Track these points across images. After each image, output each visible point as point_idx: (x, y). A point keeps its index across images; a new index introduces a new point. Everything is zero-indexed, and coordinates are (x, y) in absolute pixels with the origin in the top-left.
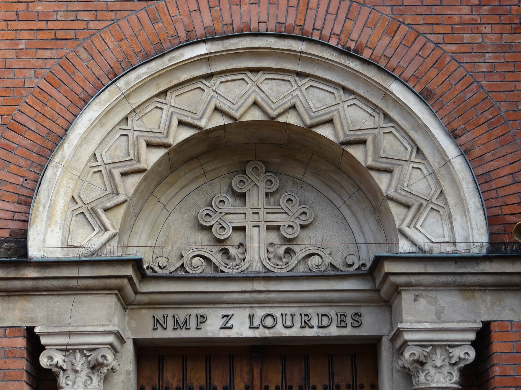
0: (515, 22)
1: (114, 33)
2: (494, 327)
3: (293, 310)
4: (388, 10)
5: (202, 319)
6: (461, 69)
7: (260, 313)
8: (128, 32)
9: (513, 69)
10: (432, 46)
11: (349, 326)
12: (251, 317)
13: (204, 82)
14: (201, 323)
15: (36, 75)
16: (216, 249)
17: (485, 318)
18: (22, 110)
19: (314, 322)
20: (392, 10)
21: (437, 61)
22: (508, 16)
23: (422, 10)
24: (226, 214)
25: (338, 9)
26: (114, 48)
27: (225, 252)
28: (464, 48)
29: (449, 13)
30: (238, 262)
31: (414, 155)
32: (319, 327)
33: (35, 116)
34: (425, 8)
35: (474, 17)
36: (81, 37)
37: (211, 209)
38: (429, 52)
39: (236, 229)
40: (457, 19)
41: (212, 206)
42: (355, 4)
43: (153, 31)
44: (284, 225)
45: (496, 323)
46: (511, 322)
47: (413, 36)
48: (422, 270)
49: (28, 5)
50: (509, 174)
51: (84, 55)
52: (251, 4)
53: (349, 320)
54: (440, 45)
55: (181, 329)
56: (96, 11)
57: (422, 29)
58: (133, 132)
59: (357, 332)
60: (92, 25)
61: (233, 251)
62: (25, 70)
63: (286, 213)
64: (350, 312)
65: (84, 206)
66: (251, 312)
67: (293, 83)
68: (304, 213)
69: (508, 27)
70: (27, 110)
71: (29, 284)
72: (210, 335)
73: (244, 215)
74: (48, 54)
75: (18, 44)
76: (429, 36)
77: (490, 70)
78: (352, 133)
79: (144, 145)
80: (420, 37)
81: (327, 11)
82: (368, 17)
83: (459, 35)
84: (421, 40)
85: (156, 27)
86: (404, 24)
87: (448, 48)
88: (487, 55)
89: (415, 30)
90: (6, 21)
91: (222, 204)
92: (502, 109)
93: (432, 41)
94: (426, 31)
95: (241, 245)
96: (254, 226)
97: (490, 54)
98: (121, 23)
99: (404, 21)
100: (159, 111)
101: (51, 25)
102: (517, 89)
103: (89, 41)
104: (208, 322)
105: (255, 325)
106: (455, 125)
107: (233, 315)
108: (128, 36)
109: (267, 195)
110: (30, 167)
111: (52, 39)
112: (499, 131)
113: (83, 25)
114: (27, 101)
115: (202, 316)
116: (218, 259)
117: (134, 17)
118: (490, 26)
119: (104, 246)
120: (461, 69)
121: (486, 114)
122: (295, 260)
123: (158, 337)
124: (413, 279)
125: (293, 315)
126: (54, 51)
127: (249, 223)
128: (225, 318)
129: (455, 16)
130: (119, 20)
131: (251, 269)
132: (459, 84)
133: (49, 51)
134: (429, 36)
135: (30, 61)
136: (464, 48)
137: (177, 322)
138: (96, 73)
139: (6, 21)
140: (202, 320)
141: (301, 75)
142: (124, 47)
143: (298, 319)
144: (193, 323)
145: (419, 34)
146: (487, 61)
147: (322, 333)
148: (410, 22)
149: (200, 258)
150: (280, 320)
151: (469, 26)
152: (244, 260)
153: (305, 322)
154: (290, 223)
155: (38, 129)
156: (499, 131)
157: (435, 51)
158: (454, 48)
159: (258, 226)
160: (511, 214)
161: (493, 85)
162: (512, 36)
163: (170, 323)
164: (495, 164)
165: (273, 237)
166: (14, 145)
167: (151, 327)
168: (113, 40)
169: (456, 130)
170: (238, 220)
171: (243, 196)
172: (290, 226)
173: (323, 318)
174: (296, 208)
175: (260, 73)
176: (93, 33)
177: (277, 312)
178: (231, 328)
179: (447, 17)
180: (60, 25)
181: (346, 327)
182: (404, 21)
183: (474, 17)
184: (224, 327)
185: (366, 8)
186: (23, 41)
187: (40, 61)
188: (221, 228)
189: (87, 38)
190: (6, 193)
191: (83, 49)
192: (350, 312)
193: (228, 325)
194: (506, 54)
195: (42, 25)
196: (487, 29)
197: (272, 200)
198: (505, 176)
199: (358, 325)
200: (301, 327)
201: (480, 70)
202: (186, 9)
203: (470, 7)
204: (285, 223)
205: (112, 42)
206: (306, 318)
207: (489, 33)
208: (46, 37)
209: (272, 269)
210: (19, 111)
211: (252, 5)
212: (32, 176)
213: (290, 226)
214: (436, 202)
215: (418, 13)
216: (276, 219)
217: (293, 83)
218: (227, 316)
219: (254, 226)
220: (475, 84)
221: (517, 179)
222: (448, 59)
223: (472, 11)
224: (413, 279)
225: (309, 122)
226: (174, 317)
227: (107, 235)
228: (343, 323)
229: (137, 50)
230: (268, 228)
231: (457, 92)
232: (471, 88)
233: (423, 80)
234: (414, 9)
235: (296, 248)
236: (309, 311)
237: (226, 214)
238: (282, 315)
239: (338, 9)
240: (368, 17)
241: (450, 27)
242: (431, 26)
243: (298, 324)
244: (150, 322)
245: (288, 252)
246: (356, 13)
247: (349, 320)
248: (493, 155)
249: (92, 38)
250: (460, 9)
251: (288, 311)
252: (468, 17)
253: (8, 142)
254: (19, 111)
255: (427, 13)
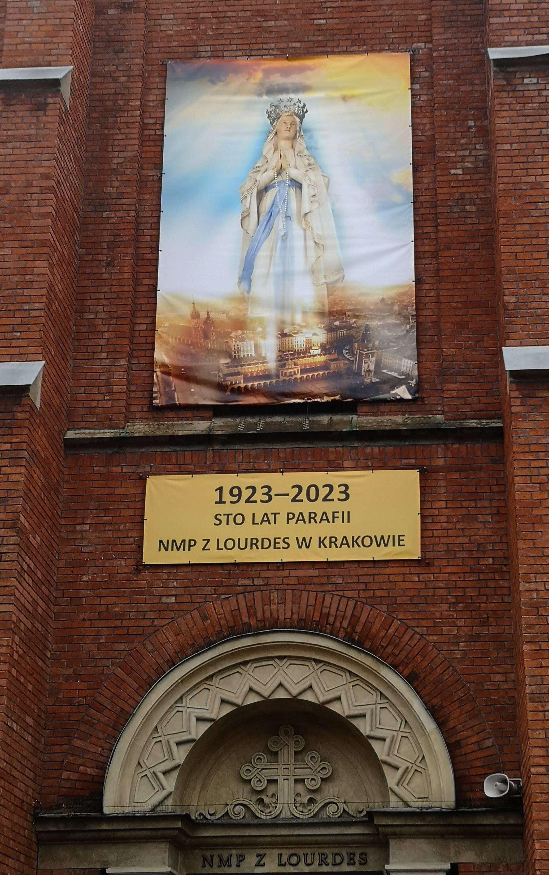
0: (484, 616)
1: (173, 629)
2: (461, 869)
3: (313, 850)
4: (384, 608)
5: (241, 859)
6: (441, 656)
7: (286, 853)
8: (184, 628)
9: (480, 656)
10: (418, 636)
11: (357, 863)
12: (280, 855)
13: (242, 667)
14: (240, 861)
15: (113, 664)
16: (254, 798)
17: (455, 861)
18: (102, 693)
19: (330, 860)
20: (388, 608)
21: (422, 649)
22: (478, 612)
23: (410, 607)
24: (263, 769)
25: (346, 607)
26: (173, 642)
27: (261, 801)
28: (442, 639)
29: (432, 610)
30: (271, 809)
31: (403, 726)
32: (333, 865)
33: (112, 697)
34: (413, 605)
35: (451, 613)
36: (148, 632)
37: (251, 765)
38: (416, 642)
39: (269, 781)
40: (438, 615)
41: (251, 763)
42: (359, 603)
43: (203, 627)
44: (308, 779)
45: (462, 865)
46: (473, 864)
47: (403, 629)
48: (403, 823)
49: (108, 607)
50: (475, 742)
51: (150, 647)
52: (280, 604)
53: (357, 858)
54: (424, 636)
55: (225, 866)
56: (160, 611)
57: (411, 623)
58: (186, 708)
59: (363, 869)
60: (156, 623)
61: (267, 800)
62: (104, 661)
63: (310, 768)
64: (358, 852)
65: (148, 770)
66: (280, 851)
67: (311, 668)
68: (324, 768)
69: (477, 621)
70: (106, 692)
71: (104, 834)
72: (247, 871)
73: (276, 770)
74: (122, 646)
75: (99, 639)
76: (416, 629)
77: (462, 656)
78: (276, 767)
79: (195, 720)
80: (409, 630)
81: (338, 609)
82: (369, 614)
83: (439, 628)
84: (410, 632)
85: (205, 624)
86: (397, 619)
87: (430, 638)
88: (461, 644)
89: (405, 624)
90: (90, 620)
91: (259, 760)
92: (471, 689)
93: (418, 633)
94: (414, 625)
95: (273, 795)
96: (284, 780)
97: (463, 644)
98: (178, 620)
99: (397, 616)
100: (207, 691)
101: (125, 623)
102: (484, 672)
103: (154, 635)
104: (246, 860)
105: (283, 862)
106: (435, 701)
107: (265, 854)
108: (183, 632)
109: (296, 753)
110: (106, 739)
111: (126, 634)
112: (468, 707)
113: (149, 623)
114: (106, 685)
115: (241, 856)
116: (255, 808)
117: (189, 616)
118: (463, 620)
119: (161, 803)
120: (441, 656)
121: (459, 693)
122: (316, 808)
123: (206, 873)
124: (398, 830)
125: (313, 855)
126: (126, 645)
127: (281, 776)
128: (259, 858)
129: (436, 613)
130: (177, 618)
131: (282, 816)
132: (439, 668)
133: (123, 644)
134: (416, 629)
135: (108, 653)
136: (442, 639)
137: (221, 860)
138: (159, 662)
139: (90, 620)
140: (241, 859)
141: (317, 661)
142: (181, 640)
143: (317, 858)
144: (234, 861)
145: (408, 627)
146: (460, 649)
147: (336, 869)
148: (401, 617)
149: (242, 807)
150: (303, 859)
151: (447, 620)
152: (276, 807)
153: (322, 860)
154: (313, 777)
155: (113, 708)
156: (468, 707)
157: (420, 641)
158: (435, 638)
159: (288, 779)
160: (476, 775)
161: (464, 668)
162: (480, 628)
163: (216, 860)
164: (465, 734)
165: (300, 788)
166: (94, 721)
167: (201, 865)
168: (172, 634)
169: (435, 706)
170: (271, 774)
171: (276, 753)
172: (313, 779)
173: (337, 857)
174: (318, 764)
175: (285, 660)
176: (157, 630)
177: (301, 852)
178: (264, 865)
179: (430, 613)
180: (133, 623)
181: (354, 864)
182: (397, 616)
183: (451, 613)
184: (258, 865)
185: (368, 606)
186: (104, 637)
187: (116, 652)
188: (258, 781)
189: (152, 633)
190: (88, 761)
191: (149, 642)
192: (358, 852)
193: (262, 863)
194: (476, 644)
195: (118, 623)
196: (461, 623)
197: (299, 757)
198: (473, 743)
199: (364, 862)
200: (319, 865)
201: (455, 656)
202: (229, 609)
203: (448, 605)
204: (309, 777)
205: (172, 637)
206: (323, 857)
207: (463, 626)
208: (120, 633)
209: (298, 816)
210: (99, 693)
211: (279, 605)
212: (107, 746)
213: (313, 779)
214: (419, 765)
215: (408, 610)
216: (301, 773)
217: (311, 668)
218: (261, 855)
219: (284, 780)
220: (451, 668)
221: (481, 746)
222: (430, 648)
223: (450, 608)
224: (398, 830)
225: (322, 699)
226: (219, 856)
227: (164, 793)
228: (352, 861)
229: (191, 643)
230: (296, 781)
231: (437, 675)
232: (447, 671)
233: (410, 666)
234: (405, 606)
235: (317, 797)
236: (326, 851)
237: (263, 769)
238: (304, 854)
239: (346, 607)
240: (369, 614)
241: (432, 621)
242: (417, 621)
243: (317, 862)
244: (200, 860)
245: (311, 801)
246: (360, 610)
247: (357, 858)
248: (463, 727)
249: (156, 633)
250: (441, 607)
251: (309, 851)
252: (447, 613)
253: (90, 719)
254: (99, 693)
255: (415, 610)
